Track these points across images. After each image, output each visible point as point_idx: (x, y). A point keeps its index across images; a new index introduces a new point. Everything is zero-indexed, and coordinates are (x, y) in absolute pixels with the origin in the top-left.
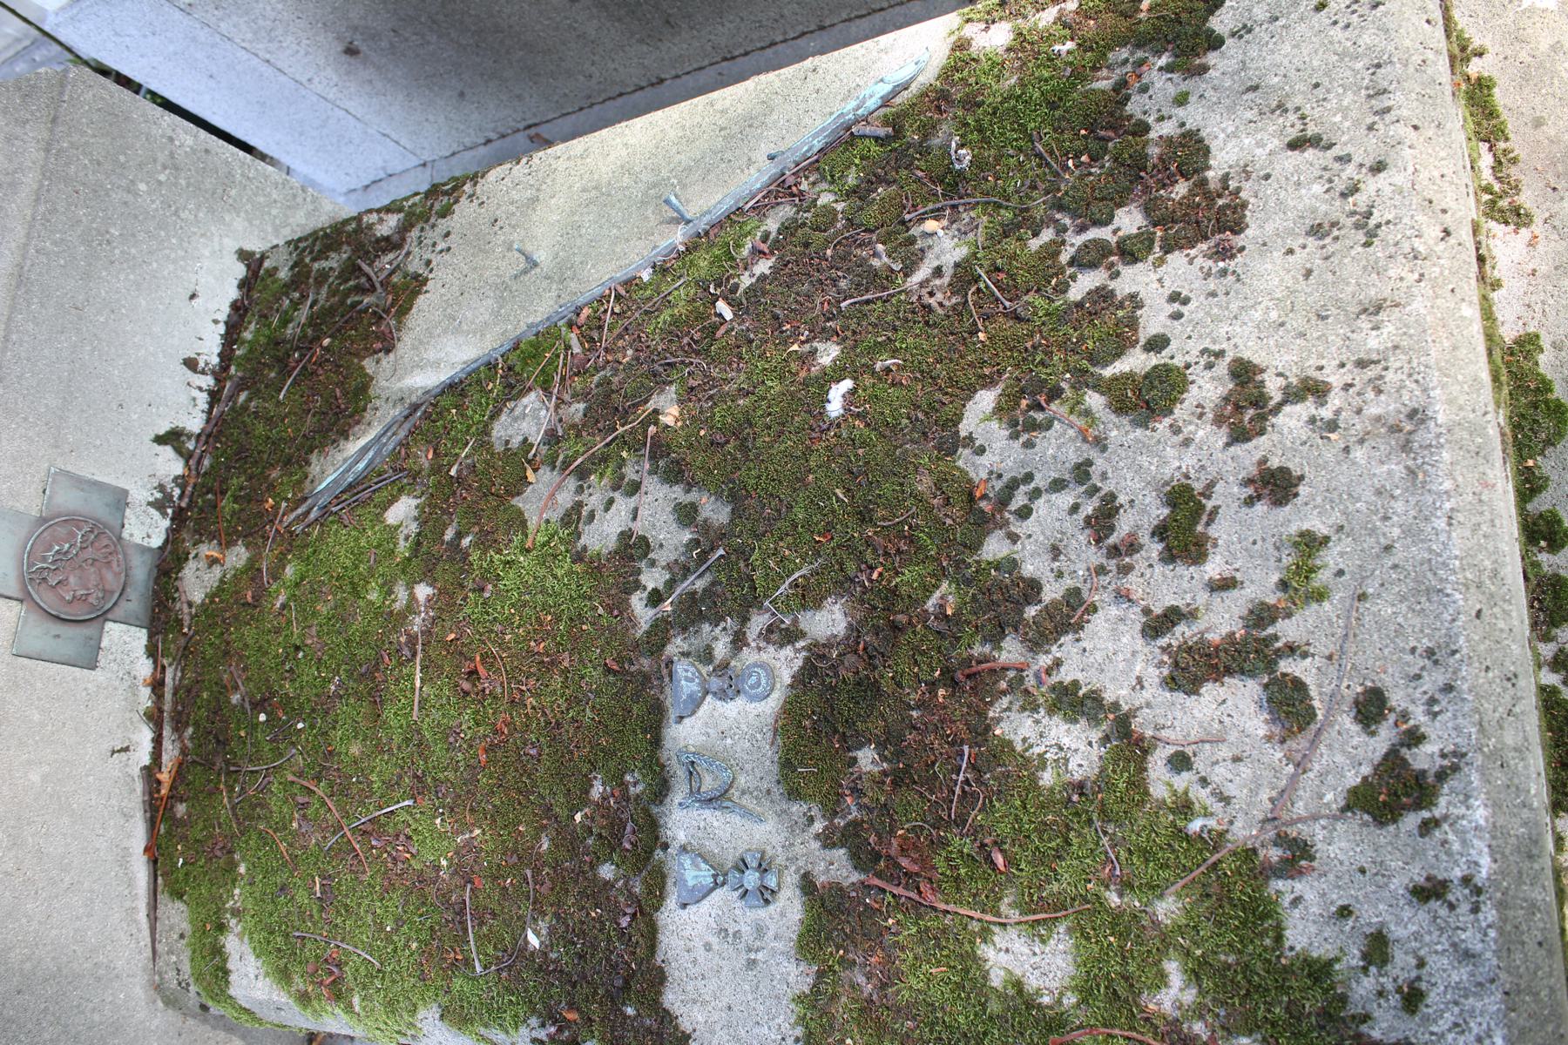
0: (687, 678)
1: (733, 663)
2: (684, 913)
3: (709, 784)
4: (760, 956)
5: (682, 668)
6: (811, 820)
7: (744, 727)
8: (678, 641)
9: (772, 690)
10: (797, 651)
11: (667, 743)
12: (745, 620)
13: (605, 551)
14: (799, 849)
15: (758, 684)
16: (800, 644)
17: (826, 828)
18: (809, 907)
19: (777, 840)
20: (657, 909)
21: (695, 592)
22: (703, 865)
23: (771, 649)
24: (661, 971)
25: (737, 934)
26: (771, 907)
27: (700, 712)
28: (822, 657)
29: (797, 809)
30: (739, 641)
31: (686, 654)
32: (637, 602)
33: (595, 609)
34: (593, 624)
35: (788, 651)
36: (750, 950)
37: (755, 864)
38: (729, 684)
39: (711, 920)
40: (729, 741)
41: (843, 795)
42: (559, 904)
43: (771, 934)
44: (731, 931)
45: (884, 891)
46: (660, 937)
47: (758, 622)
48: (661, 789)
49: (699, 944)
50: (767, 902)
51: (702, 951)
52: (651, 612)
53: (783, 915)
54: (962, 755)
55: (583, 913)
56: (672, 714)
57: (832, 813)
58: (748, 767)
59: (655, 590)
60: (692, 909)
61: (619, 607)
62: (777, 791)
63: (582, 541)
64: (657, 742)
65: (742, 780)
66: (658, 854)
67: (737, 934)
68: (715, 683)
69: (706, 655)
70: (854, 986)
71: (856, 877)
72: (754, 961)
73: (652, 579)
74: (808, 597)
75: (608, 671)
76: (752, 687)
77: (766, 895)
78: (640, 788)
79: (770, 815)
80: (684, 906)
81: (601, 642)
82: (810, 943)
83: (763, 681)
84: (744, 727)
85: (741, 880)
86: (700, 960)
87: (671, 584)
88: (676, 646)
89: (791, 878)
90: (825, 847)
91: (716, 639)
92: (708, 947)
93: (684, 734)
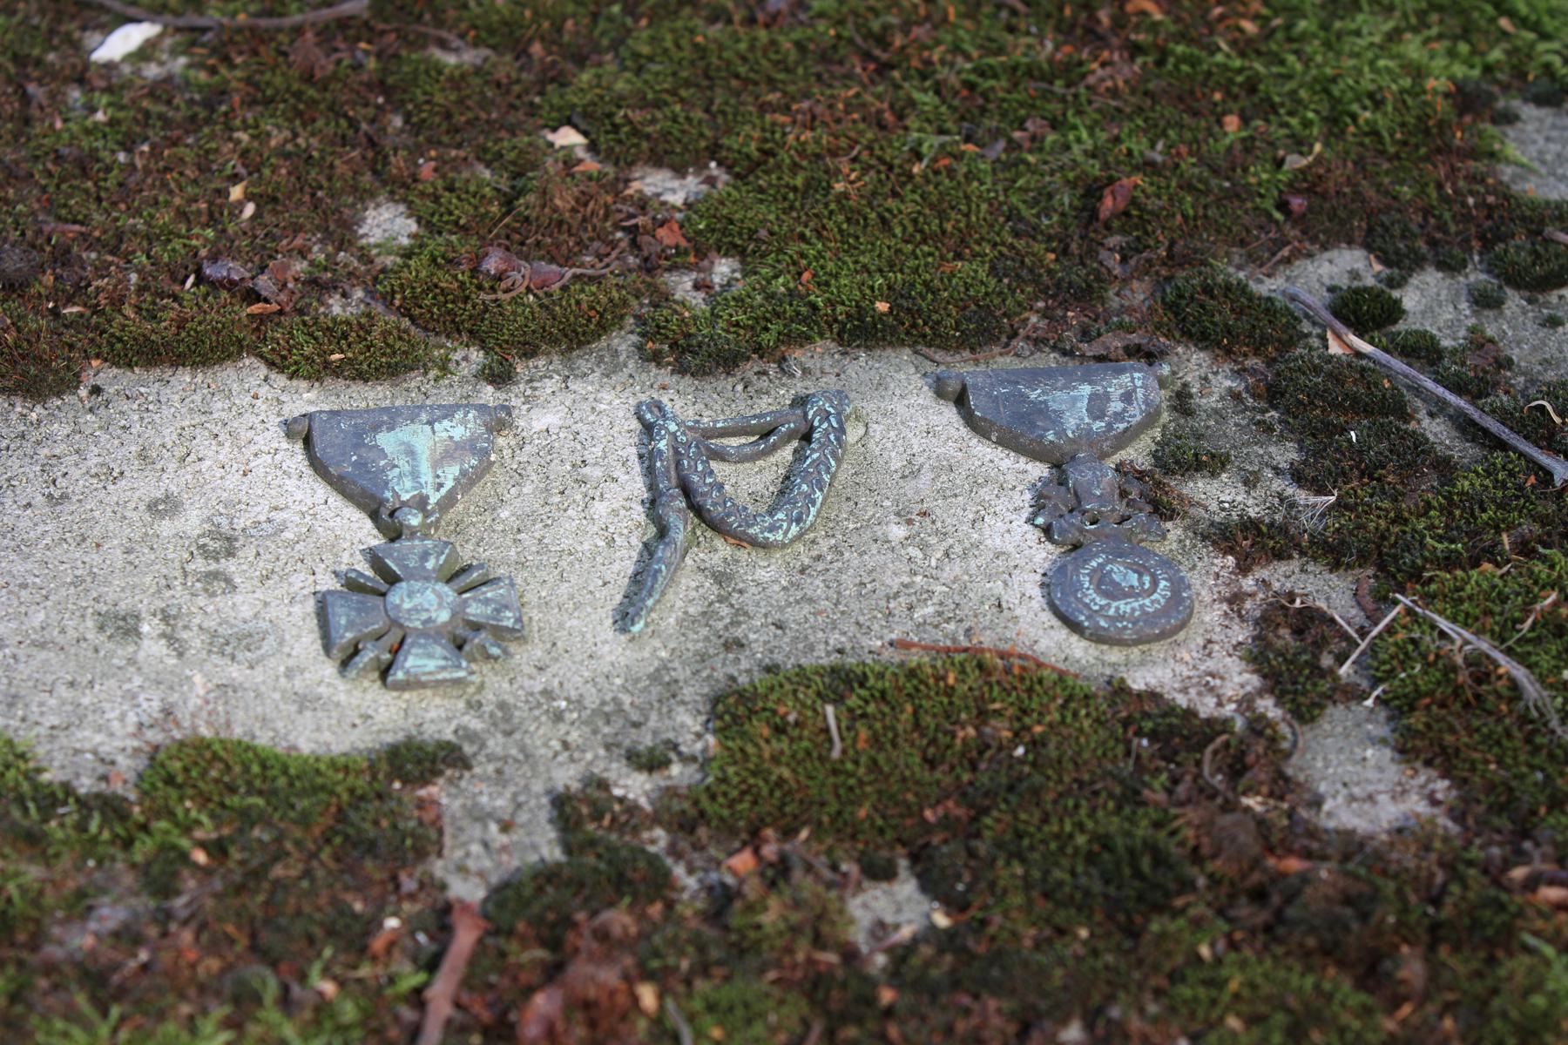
0: (1109, 403)
1: (1174, 530)
4: (153, 648)
5: (1132, 390)
6: (652, 762)
7: (952, 570)
8: (1225, 382)
9: (1098, 638)
10: (1246, 703)
11: (862, 366)
12: (1332, 552)
13: (1507, 173)
15: (1114, 592)
16: (1268, 707)
17: (632, 809)
21: (1406, 417)
22: (450, 474)
24: (66, 383)
26: (329, 669)
27: (986, 453)
28: (1237, 768)
29: (688, 726)
30: (1249, 541)
31: (1182, 402)
32: (1346, 265)
33: (1300, 144)
34: (1248, 145)
35: (1239, 679)
37: (475, 611)
40: (898, 532)
41: (754, 840)
42: (260, 98)
44: (229, 566)
45: (432, 965)
46: (184, 376)
47: (1332, 593)
48: (687, 351)
49: (173, 482)
53: (304, 702)
55: (234, 164)
56: (962, 367)
57: (685, 819)
58: (815, 587)
60: (295, 458)
61: (1320, 216)
62: (744, 670)
63: (1529, 111)
64: (861, 332)
65: (765, 572)
68: (1097, 480)
69: (1184, 458)
70: (80, 905)
73: (1431, 302)
74: (1438, 718)
75: (1092, 192)
81: (1188, 165)
82: (207, 777)
83: (1124, 606)
84: (952, 570)
86: (117, 491)
87: (1422, 350)
89: (437, 717)
90: (561, 803)
91: (1250, 482)
92: (164, 507)
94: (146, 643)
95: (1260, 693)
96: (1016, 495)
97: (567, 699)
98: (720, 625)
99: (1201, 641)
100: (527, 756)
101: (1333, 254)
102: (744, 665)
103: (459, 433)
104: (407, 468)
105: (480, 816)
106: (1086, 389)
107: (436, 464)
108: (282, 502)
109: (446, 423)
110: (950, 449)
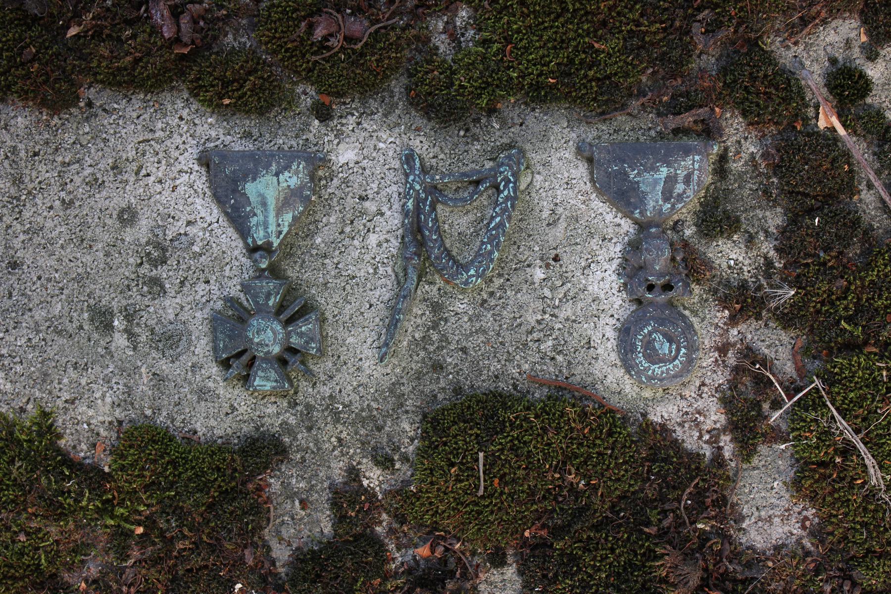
0: (678, 181)
2: (188, 160)
3: (456, 221)
4: (120, 340)
5: (694, 167)
6: (385, 462)
7: (567, 311)
8: (751, 148)
10: (714, 436)
11: (536, 120)
12: (786, 319)
14: (329, 433)
16: (728, 448)
17: (370, 494)
18: (216, 450)
19: (346, 382)
20: (195, 93)
22: (288, 217)
23: (721, 378)
25: (156, 286)
26: (214, 369)
30: (742, 301)
31: (721, 168)
35: (716, 417)
36: (129, 317)
37: (295, 340)
38: (660, 279)
39: (180, 226)
40: (539, 274)
43: (164, 366)
44: (162, 272)
47: (778, 346)
48: (444, 103)
49: (130, 196)
50: (226, 364)
51: (118, 202)
52: (814, 78)
54: (477, 460)
59: (863, 85)
64: (539, 95)
66: (307, 95)
67: (156, 286)
69: (716, 219)
71: (281, 554)
72: (108, 327)
74: (821, 476)
76: (649, 344)
77: (239, 362)
78: (441, 43)
79: (393, 368)
80: (205, 160)
82: (148, 445)
84: (567, 311)
85: (261, 310)
88: (743, 142)
89: (274, 415)
91: (750, 240)
92: (128, 217)
93: (558, 169)
94: (117, 335)
95: (724, 430)
96: (611, 246)
97: (343, 404)
98: (431, 348)
99: (698, 384)
100: (319, 449)
101: (837, 22)
102: (442, 384)
103: (294, 182)
104: (261, 218)
105: (291, 496)
106: (664, 171)
107: (279, 212)
108: (191, 218)
109: (287, 174)
110: (576, 201)
